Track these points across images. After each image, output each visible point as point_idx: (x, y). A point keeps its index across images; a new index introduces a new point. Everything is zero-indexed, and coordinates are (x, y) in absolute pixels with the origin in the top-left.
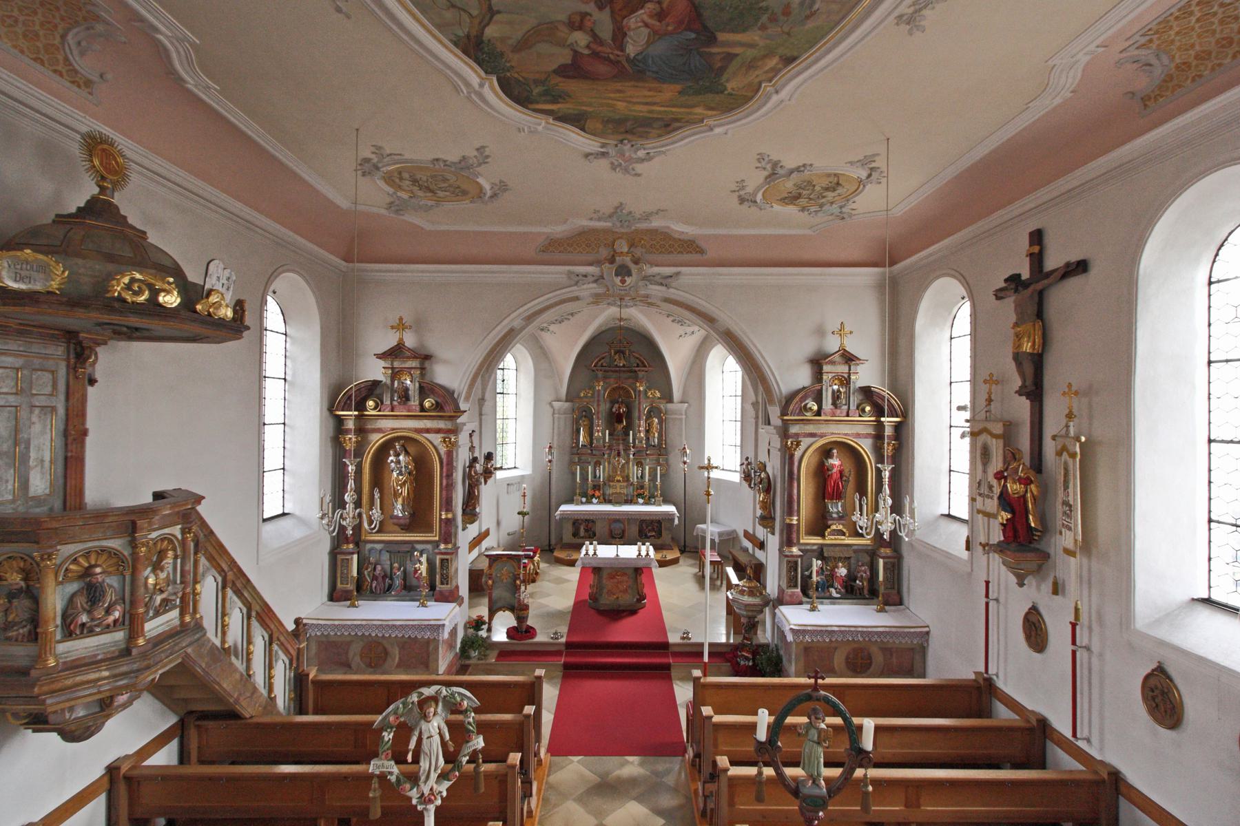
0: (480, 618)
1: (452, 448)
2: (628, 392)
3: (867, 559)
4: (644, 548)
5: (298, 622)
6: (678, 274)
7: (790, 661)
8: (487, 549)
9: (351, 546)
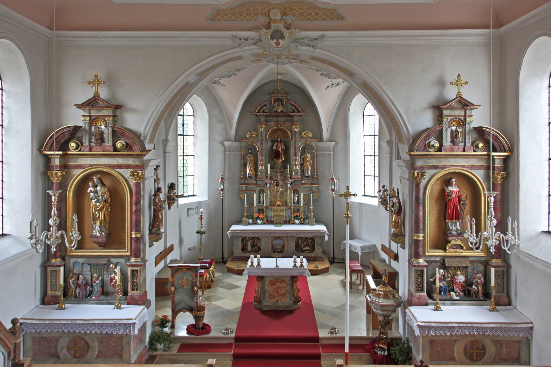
0: (165, 317)
1: (140, 180)
2: (286, 132)
3: (481, 268)
4: (298, 260)
5: (14, 322)
6: (323, 36)
7: (418, 352)
8: (171, 262)
9: (59, 260)
